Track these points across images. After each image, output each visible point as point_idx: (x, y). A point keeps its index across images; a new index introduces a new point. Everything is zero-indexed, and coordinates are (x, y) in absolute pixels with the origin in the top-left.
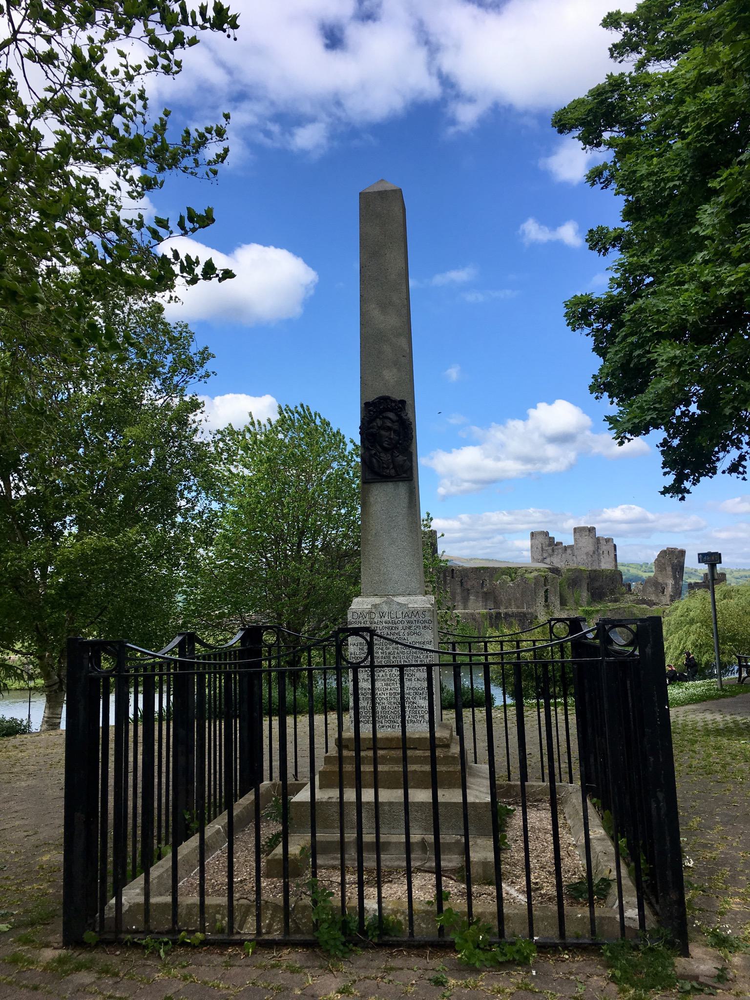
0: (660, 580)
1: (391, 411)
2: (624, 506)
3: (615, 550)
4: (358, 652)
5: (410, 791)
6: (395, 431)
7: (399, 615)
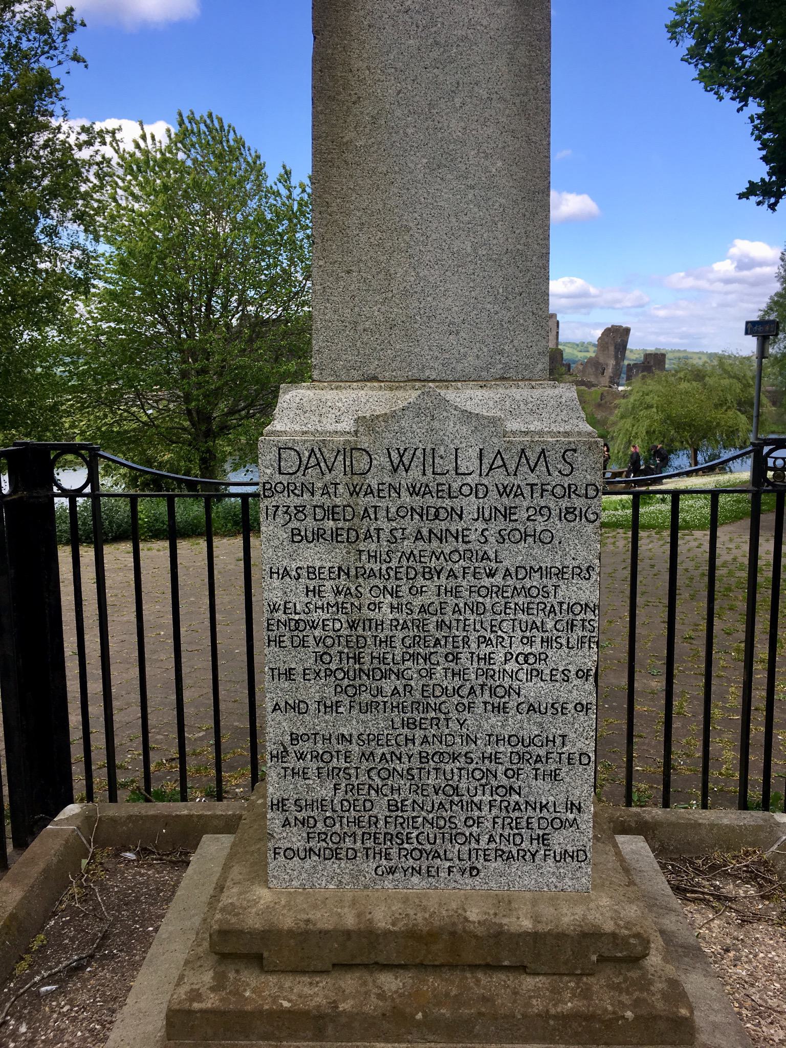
0: (601, 360)
2: (566, 279)
3: (558, 326)
4: (300, 600)
7: (468, 462)
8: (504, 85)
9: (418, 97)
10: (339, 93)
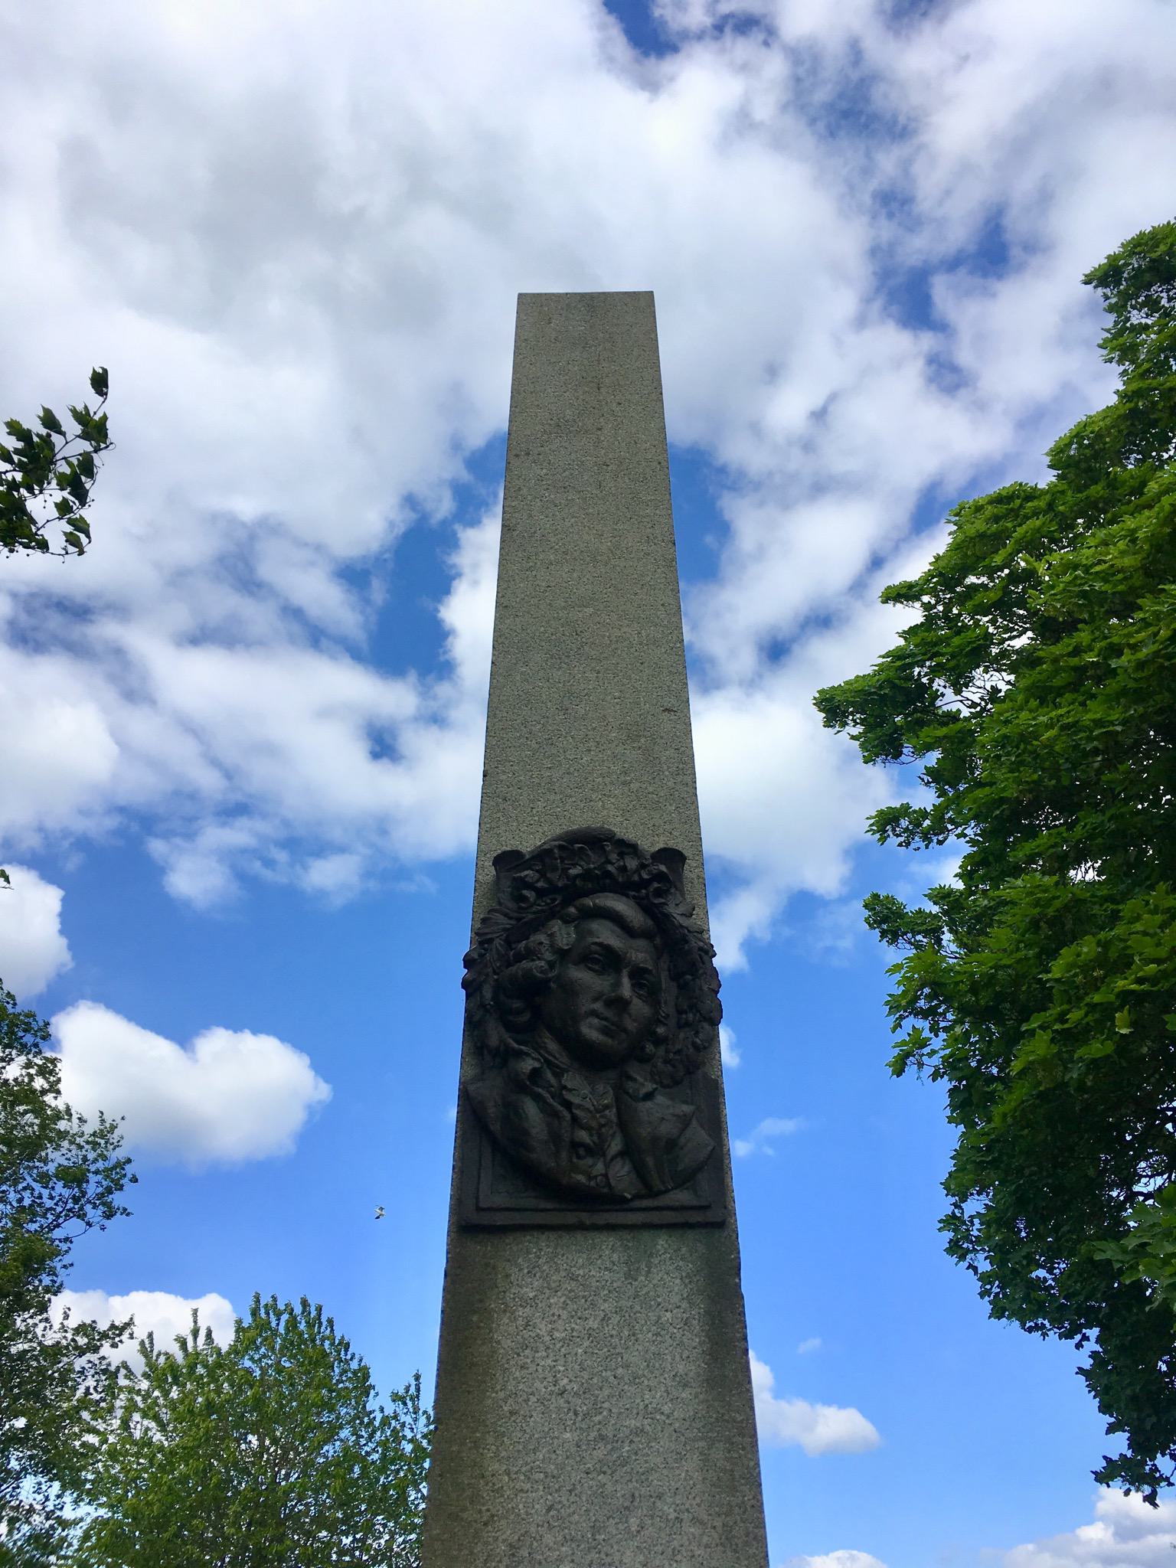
1: (622, 889)
2: (840, 1553)
6: (638, 975)
8: (698, 1500)
9: (576, 1517)
10: (464, 1509)
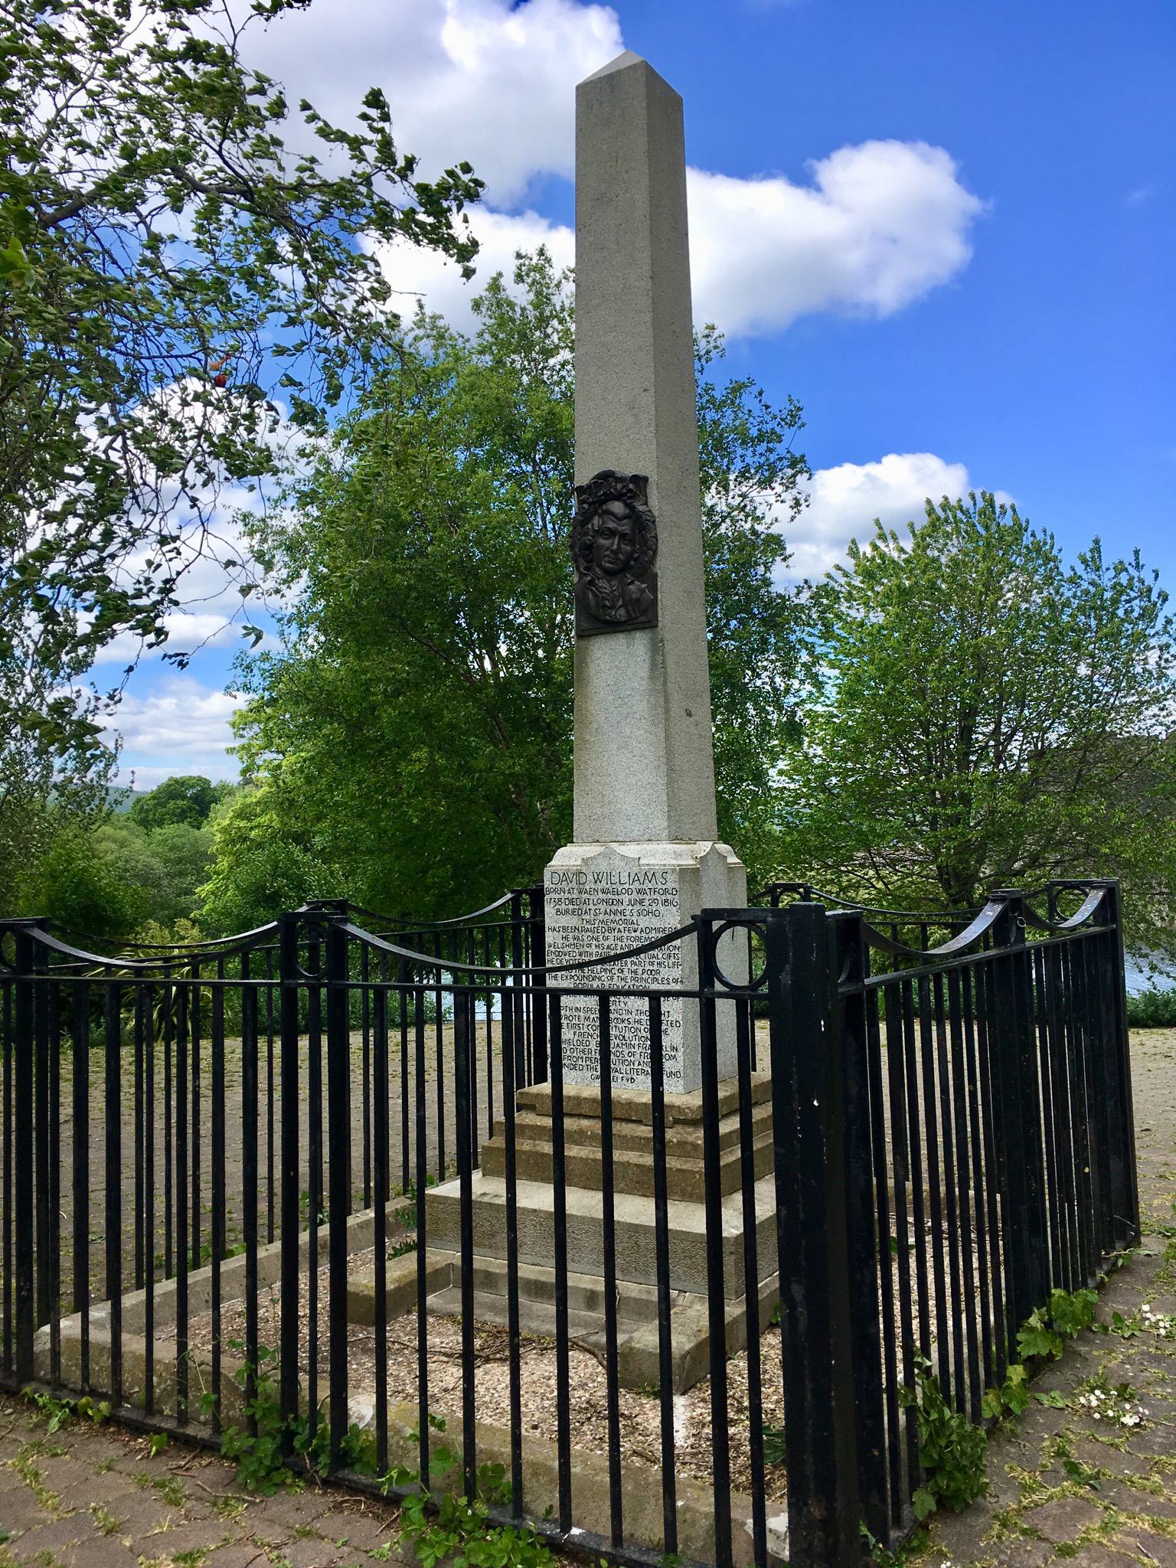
4: (560, 942)
5: (617, 1198)
